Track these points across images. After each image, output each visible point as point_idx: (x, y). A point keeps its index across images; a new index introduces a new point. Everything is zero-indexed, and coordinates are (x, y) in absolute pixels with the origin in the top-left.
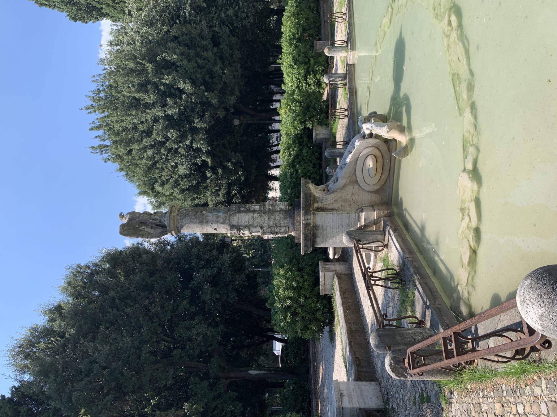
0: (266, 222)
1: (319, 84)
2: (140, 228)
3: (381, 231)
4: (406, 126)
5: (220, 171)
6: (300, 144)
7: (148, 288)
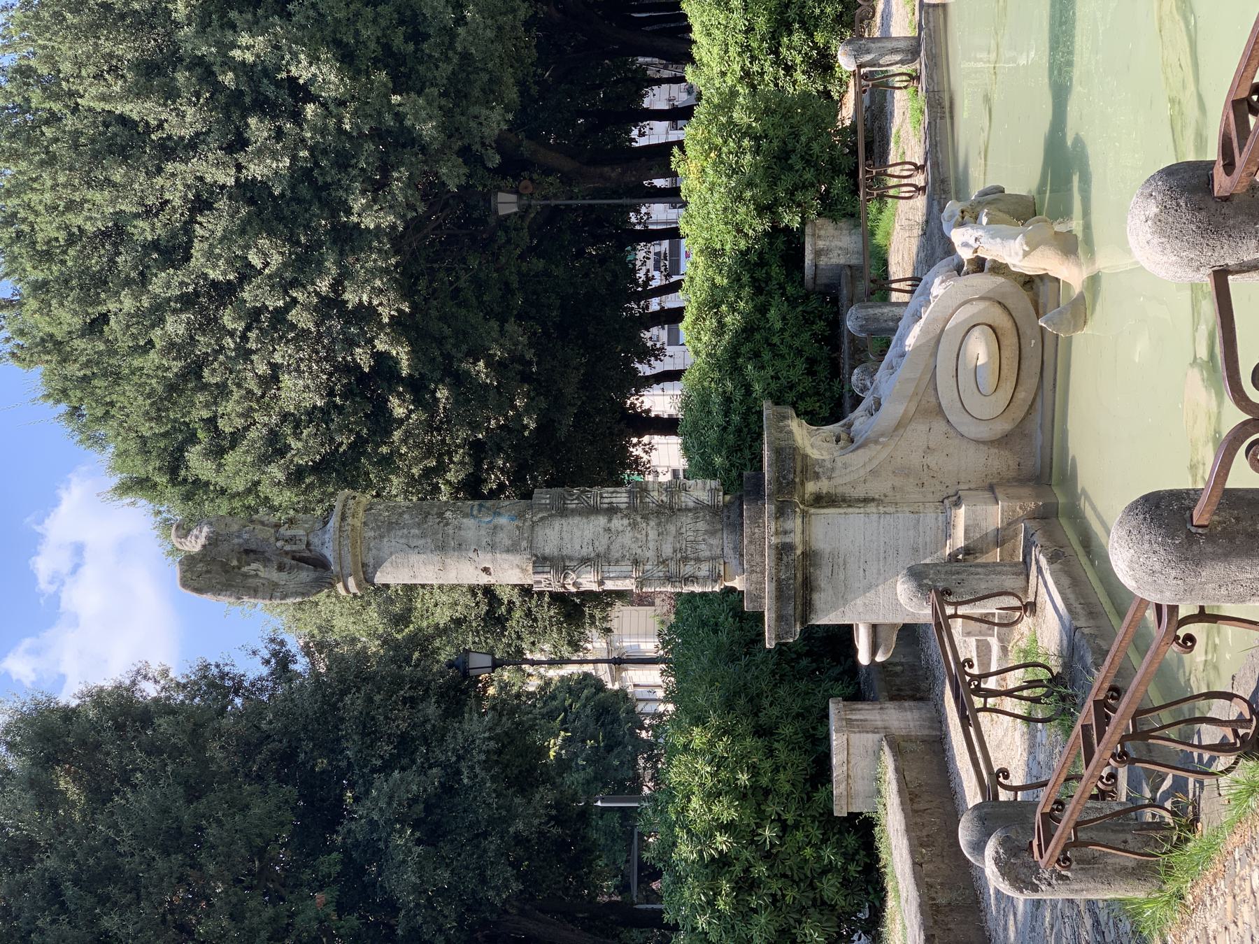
0: (651, 545)
1: (823, 64)
2: (245, 569)
3: (1016, 564)
4: (1080, 235)
5: (442, 394)
6: (759, 288)
7: (179, 840)
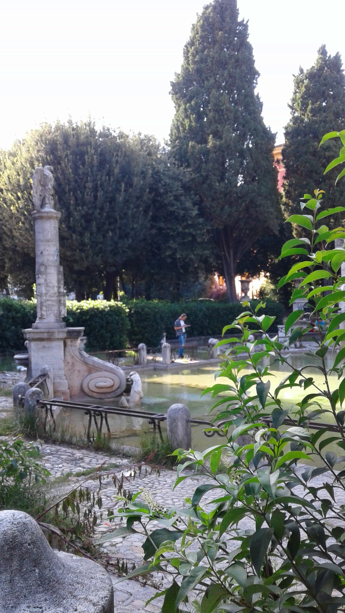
0: (50, 298)
